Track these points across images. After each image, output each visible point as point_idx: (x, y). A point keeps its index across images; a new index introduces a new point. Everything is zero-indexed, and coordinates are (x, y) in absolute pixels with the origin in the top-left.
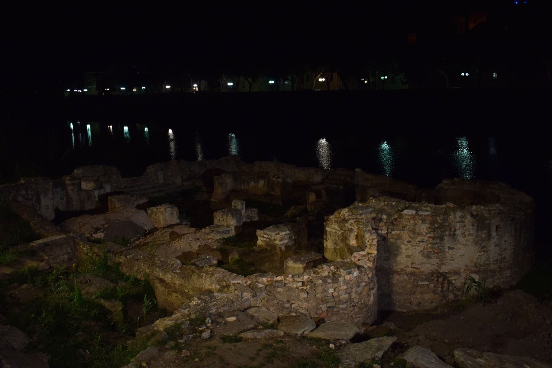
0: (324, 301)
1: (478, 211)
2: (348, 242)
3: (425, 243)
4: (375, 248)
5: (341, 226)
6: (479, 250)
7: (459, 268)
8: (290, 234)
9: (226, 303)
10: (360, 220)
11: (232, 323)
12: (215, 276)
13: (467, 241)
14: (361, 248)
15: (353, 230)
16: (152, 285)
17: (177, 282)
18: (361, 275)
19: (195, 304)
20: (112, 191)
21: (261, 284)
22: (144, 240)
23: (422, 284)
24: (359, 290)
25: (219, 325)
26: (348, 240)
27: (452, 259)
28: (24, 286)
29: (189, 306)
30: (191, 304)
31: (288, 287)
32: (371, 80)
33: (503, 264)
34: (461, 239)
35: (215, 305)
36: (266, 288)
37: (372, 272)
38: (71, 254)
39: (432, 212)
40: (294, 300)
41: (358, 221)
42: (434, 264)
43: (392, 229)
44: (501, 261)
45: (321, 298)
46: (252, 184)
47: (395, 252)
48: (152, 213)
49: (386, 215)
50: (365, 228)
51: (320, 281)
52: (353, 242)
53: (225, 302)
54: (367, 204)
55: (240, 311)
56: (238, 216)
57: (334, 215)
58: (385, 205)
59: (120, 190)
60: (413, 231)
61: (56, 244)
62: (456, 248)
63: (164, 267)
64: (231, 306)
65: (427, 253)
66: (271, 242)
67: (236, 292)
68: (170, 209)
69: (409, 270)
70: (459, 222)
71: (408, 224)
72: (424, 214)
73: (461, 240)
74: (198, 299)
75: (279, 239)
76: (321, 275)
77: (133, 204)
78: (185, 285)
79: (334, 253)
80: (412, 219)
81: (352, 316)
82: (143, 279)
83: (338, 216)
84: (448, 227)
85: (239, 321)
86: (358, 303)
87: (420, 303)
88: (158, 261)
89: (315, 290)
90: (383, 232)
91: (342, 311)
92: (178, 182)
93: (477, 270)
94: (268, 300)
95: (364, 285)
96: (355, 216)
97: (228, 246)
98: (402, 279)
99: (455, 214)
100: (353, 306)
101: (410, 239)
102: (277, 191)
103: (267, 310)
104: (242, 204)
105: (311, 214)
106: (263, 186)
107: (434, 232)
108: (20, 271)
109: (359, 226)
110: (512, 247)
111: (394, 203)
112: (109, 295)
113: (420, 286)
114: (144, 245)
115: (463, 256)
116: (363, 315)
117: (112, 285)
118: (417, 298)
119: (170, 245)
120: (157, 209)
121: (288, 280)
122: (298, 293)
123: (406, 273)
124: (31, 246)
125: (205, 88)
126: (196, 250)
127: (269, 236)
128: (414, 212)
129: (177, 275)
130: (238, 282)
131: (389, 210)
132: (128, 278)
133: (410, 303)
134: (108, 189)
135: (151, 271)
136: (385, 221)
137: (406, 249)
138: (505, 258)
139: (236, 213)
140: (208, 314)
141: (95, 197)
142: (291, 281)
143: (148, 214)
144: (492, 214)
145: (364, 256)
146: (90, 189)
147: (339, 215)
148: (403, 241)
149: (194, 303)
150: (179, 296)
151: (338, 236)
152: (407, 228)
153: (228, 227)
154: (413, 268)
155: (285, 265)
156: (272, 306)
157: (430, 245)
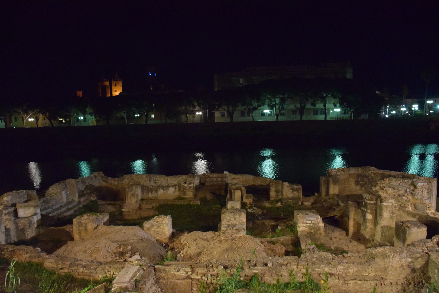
66: (315, 226)
79: (390, 220)
141: (34, 223)
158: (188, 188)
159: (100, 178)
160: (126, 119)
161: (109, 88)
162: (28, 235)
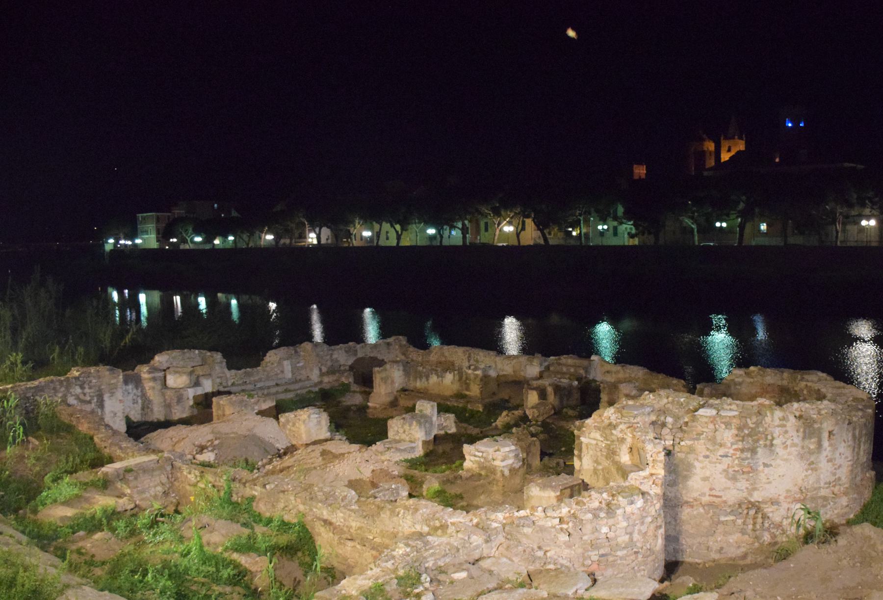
0: (594, 545)
1: (802, 411)
2: (617, 458)
3: (730, 458)
4: (662, 465)
5: (606, 435)
6: (806, 467)
7: (777, 495)
8: (516, 449)
9: (448, 552)
10: (635, 425)
11: (462, 581)
12: (421, 511)
13: (790, 454)
14: (637, 466)
15: (625, 439)
16: (310, 530)
17: (354, 524)
18: (646, 506)
19: (402, 554)
20: (214, 390)
21: (496, 522)
22: (279, 463)
23: (726, 519)
24: (644, 529)
25: (442, 585)
26: (618, 455)
27: (768, 481)
28: (98, 536)
29: (393, 557)
30: (395, 553)
31: (540, 526)
32: (584, 230)
33: (837, 488)
34: (779, 450)
35: (432, 554)
36: (504, 528)
37: (659, 502)
38: (168, 486)
39: (741, 412)
40: (548, 545)
41: (632, 426)
42: (742, 490)
43: (680, 438)
44: (834, 483)
45: (589, 541)
46: (434, 379)
47: (685, 473)
48: (288, 421)
49: (671, 417)
50: (644, 437)
51: (590, 516)
52: (625, 458)
53: (447, 549)
54: (641, 402)
55: (470, 563)
56: (427, 425)
57: (592, 418)
58: (668, 403)
59: (226, 389)
60: (713, 440)
61: (144, 469)
62: (773, 464)
63: (329, 499)
64: (455, 556)
65: (733, 473)
66: (487, 463)
67: (460, 535)
68: (317, 416)
69: (706, 499)
70: (778, 426)
71: (705, 430)
72: (729, 415)
73: (780, 454)
74: (405, 545)
75: (500, 458)
76: (588, 506)
77: (254, 410)
78: (368, 529)
79: (593, 476)
80: (712, 422)
81: (634, 568)
82: (295, 521)
83: (599, 420)
84: (764, 433)
85: (473, 578)
86: (642, 548)
87: (722, 548)
88: (318, 491)
89: (580, 529)
90: (667, 442)
91: (621, 560)
92: (315, 376)
93: (802, 498)
94: (508, 548)
95: (650, 521)
96: (627, 419)
97: (416, 471)
98: (695, 513)
99: (772, 414)
100: (636, 553)
101: (708, 453)
102: (475, 390)
103: (510, 562)
104: (432, 406)
105: (534, 422)
106: (452, 383)
107: (743, 441)
108: (89, 512)
109: (635, 433)
110: (850, 463)
111: (682, 400)
112: (248, 547)
113: (722, 522)
114: (281, 471)
115: (783, 476)
116: (648, 566)
117: (246, 531)
118: (717, 541)
119: (328, 470)
120: (296, 416)
121: (538, 516)
122: (555, 535)
123: (701, 503)
124: (103, 472)
125: (327, 239)
126: (368, 478)
127: (484, 454)
128: (714, 412)
129: (355, 513)
130: (459, 520)
131: (675, 410)
132: (270, 521)
133: (708, 550)
134: (208, 386)
135: (307, 508)
136: (670, 426)
137: (702, 468)
138: (839, 479)
139: (424, 420)
140: (423, 569)
141: (188, 399)
142: (542, 517)
143: (281, 424)
144: (822, 415)
145: (645, 478)
146: (180, 387)
147: (601, 419)
148: (697, 455)
149: (401, 552)
150: (358, 546)
151: (601, 450)
152: (704, 436)
153: (411, 442)
154: (712, 496)
155: (527, 494)
156: (516, 555)
157: (736, 462)
158: (472, 377)
159: (397, 347)
160: (696, 233)
161: (713, 157)
162: (175, 413)
